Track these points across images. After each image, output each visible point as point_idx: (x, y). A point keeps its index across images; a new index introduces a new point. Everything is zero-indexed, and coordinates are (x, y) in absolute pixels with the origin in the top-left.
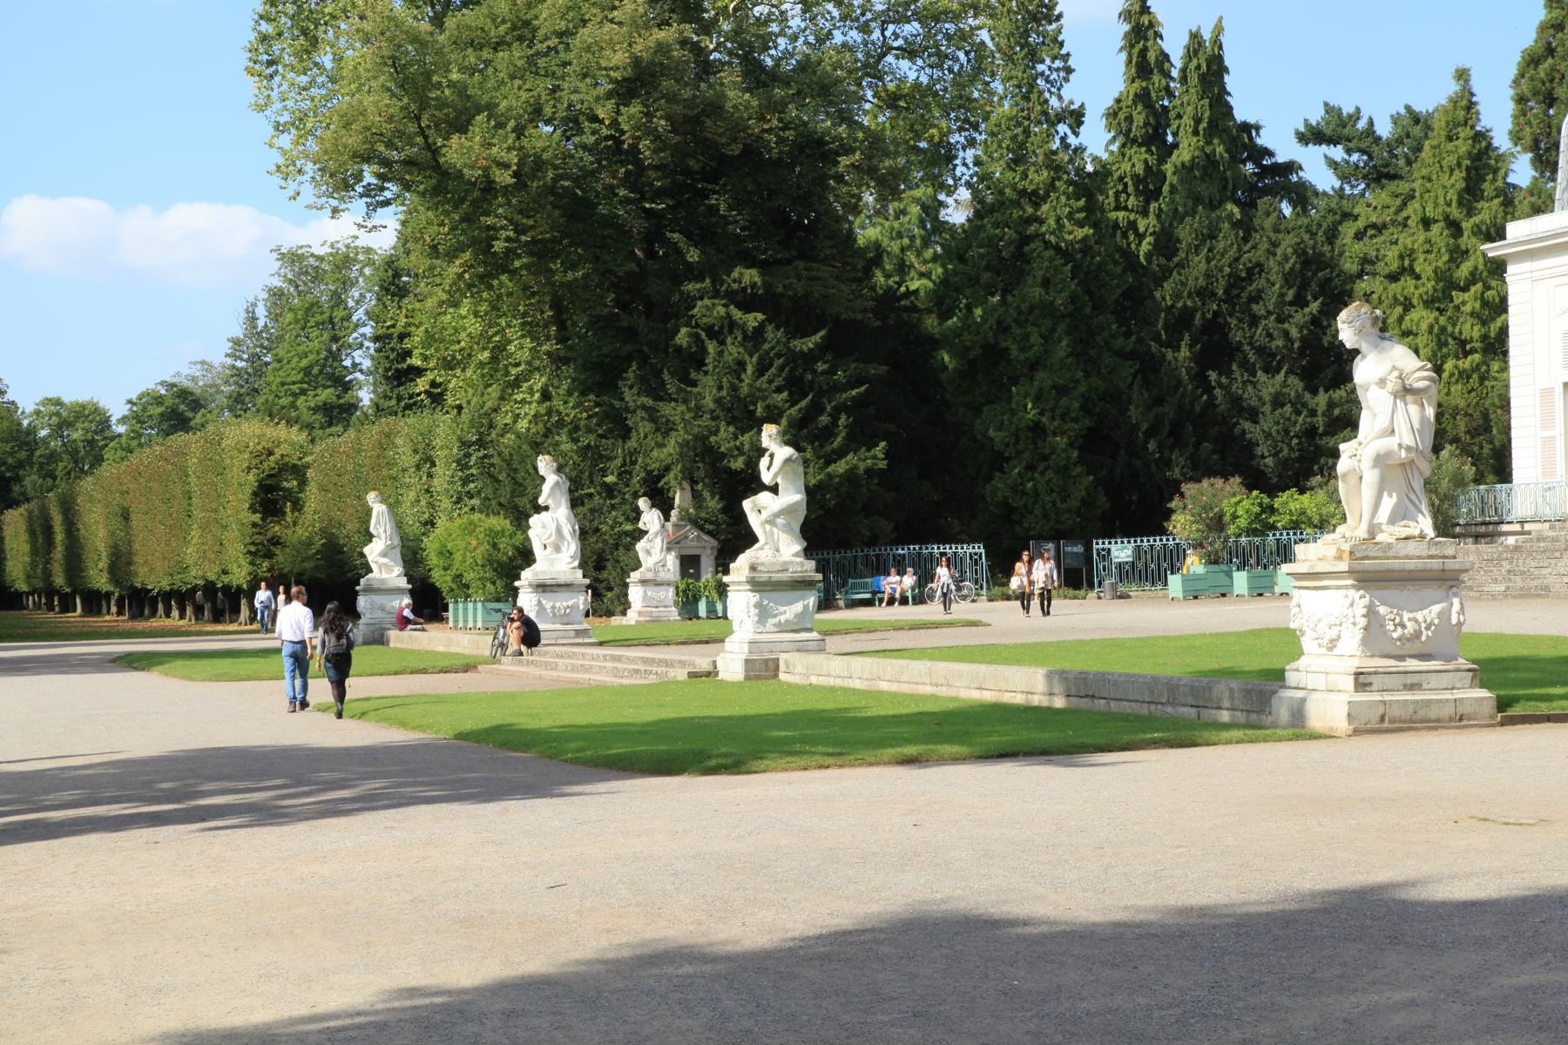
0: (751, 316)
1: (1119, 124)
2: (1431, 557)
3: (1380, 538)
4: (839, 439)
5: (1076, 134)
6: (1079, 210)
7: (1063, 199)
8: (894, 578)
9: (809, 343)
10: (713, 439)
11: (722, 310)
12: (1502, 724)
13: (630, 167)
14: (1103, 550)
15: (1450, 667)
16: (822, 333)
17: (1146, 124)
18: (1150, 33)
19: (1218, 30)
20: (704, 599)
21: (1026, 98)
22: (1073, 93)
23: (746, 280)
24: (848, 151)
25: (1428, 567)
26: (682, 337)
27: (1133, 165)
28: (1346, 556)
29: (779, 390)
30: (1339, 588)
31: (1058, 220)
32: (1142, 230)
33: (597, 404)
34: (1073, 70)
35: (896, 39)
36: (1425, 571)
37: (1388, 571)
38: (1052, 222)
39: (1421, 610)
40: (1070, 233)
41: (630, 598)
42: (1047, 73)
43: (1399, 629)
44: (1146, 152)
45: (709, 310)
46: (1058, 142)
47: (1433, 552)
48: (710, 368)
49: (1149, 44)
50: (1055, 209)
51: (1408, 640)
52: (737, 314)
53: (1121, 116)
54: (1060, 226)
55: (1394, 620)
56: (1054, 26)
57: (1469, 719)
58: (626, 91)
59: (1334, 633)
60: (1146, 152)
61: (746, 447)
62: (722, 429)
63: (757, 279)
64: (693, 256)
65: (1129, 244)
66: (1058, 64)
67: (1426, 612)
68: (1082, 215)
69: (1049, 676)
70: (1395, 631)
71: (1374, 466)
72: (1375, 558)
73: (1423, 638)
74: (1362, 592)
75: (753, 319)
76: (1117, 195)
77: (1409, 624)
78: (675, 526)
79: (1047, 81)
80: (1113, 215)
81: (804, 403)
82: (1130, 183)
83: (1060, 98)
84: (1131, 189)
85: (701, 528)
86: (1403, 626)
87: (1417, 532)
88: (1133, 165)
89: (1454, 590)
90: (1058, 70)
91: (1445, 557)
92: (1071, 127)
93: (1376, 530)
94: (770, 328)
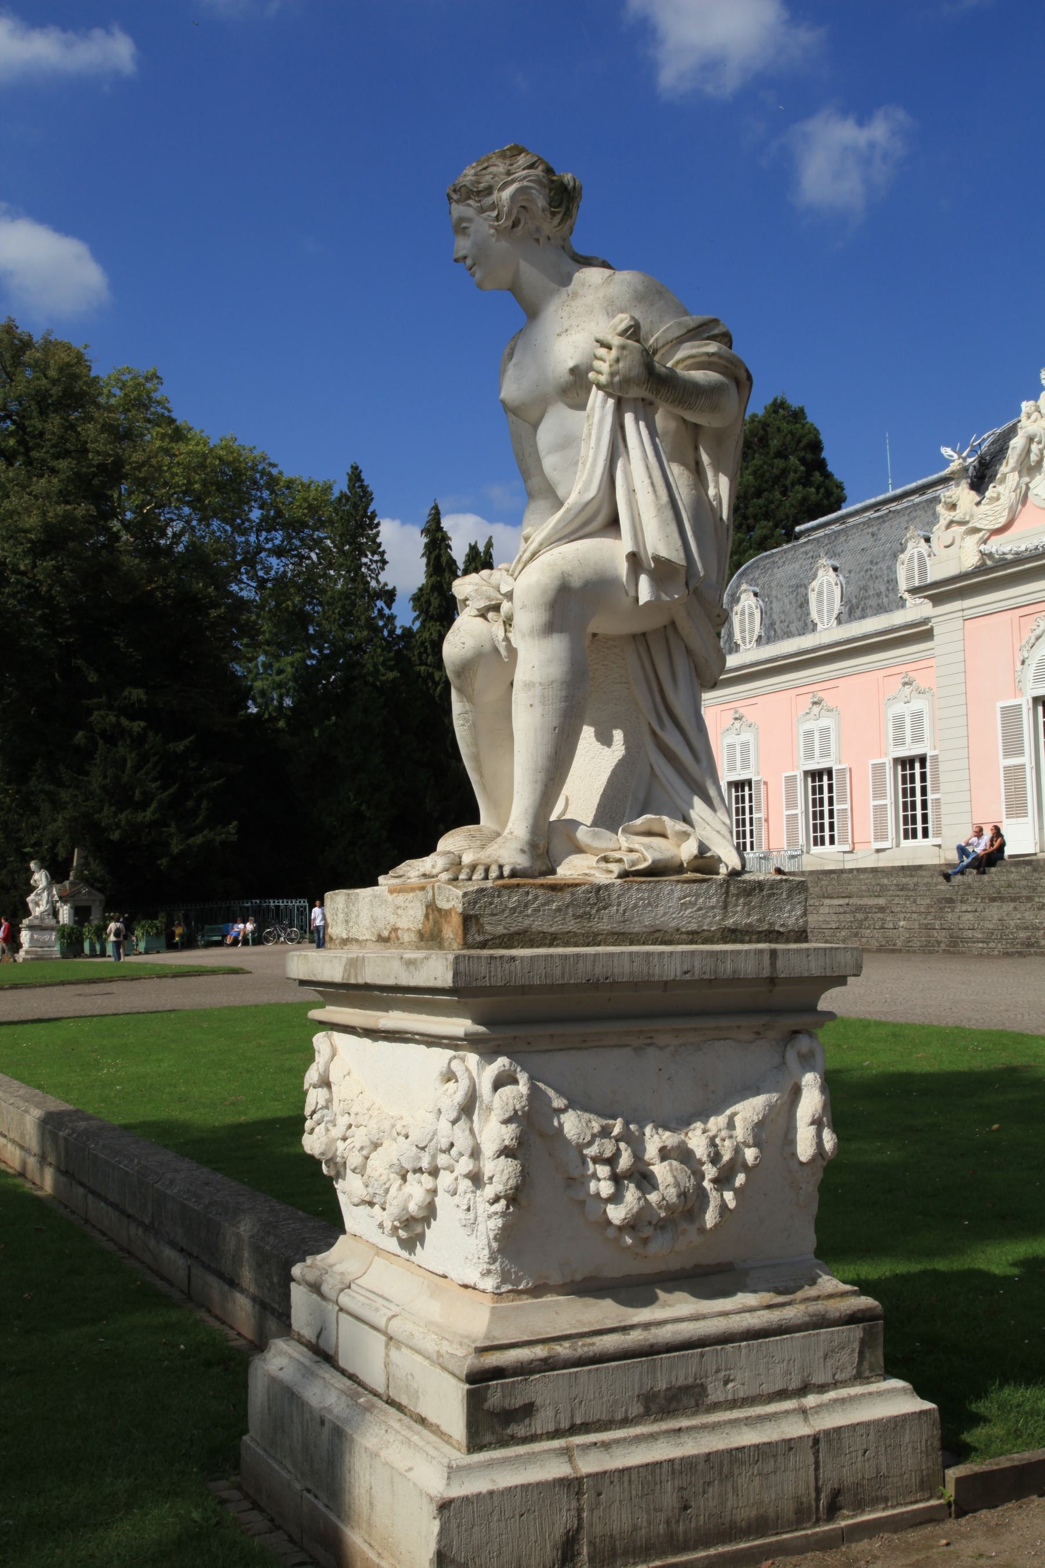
0: (135, 724)
1: (421, 605)
2: (732, 934)
3: (571, 868)
4: (200, 818)
5: (390, 608)
6: (391, 659)
7: (379, 651)
8: (241, 926)
9: (180, 746)
10: (96, 816)
11: (113, 719)
12: (961, 1508)
13: (46, 611)
14: (301, 907)
15: (791, 1314)
16: (192, 738)
17: (440, 606)
18: (443, 545)
19: (489, 545)
20: (88, 940)
21: (353, 580)
22: (388, 578)
23: (134, 697)
24: (216, 606)
25: (727, 968)
26: (80, 737)
27: (431, 634)
28: (451, 930)
29: (154, 780)
30: (432, 1041)
31: (375, 665)
32: (437, 679)
33: (18, 792)
34: (387, 562)
35: (267, 543)
36: (714, 982)
37: (593, 985)
38: (370, 667)
39: (704, 1115)
40: (384, 675)
41: (22, 941)
42: (369, 563)
43: (631, 1194)
44: (440, 625)
45: (102, 718)
46: (376, 612)
47: (737, 917)
48: (98, 761)
49: (442, 552)
50: (372, 657)
51: (661, 1226)
52: (125, 722)
53: (423, 600)
54: (377, 671)
55: (611, 1161)
56: (374, 531)
57: (860, 1506)
58: (41, 549)
59: (415, 1191)
60: (440, 625)
61: (123, 823)
62: (105, 809)
63: (143, 697)
64: (93, 677)
65: (428, 689)
66: (376, 557)
67: (718, 1121)
68: (392, 663)
69: (50, 1123)
70: (616, 1198)
71: (551, 627)
72: (552, 939)
73: (710, 1218)
74: (502, 1062)
75: (138, 726)
76: (420, 654)
77: (661, 1171)
78: (72, 884)
79: (369, 569)
80: (418, 668)
81: (171, 791)
82: (429, 646)
83: (378, 582)
84: (429, 650)
85: (92, 886)
86: (644, 1179)
87: (687, 851)
88: (431, 634)
89: (803, 1043)
90: (376, 562)
91: (771, 935)
92: (385, 602)
93: (558, 845)
94: (151, 734)
